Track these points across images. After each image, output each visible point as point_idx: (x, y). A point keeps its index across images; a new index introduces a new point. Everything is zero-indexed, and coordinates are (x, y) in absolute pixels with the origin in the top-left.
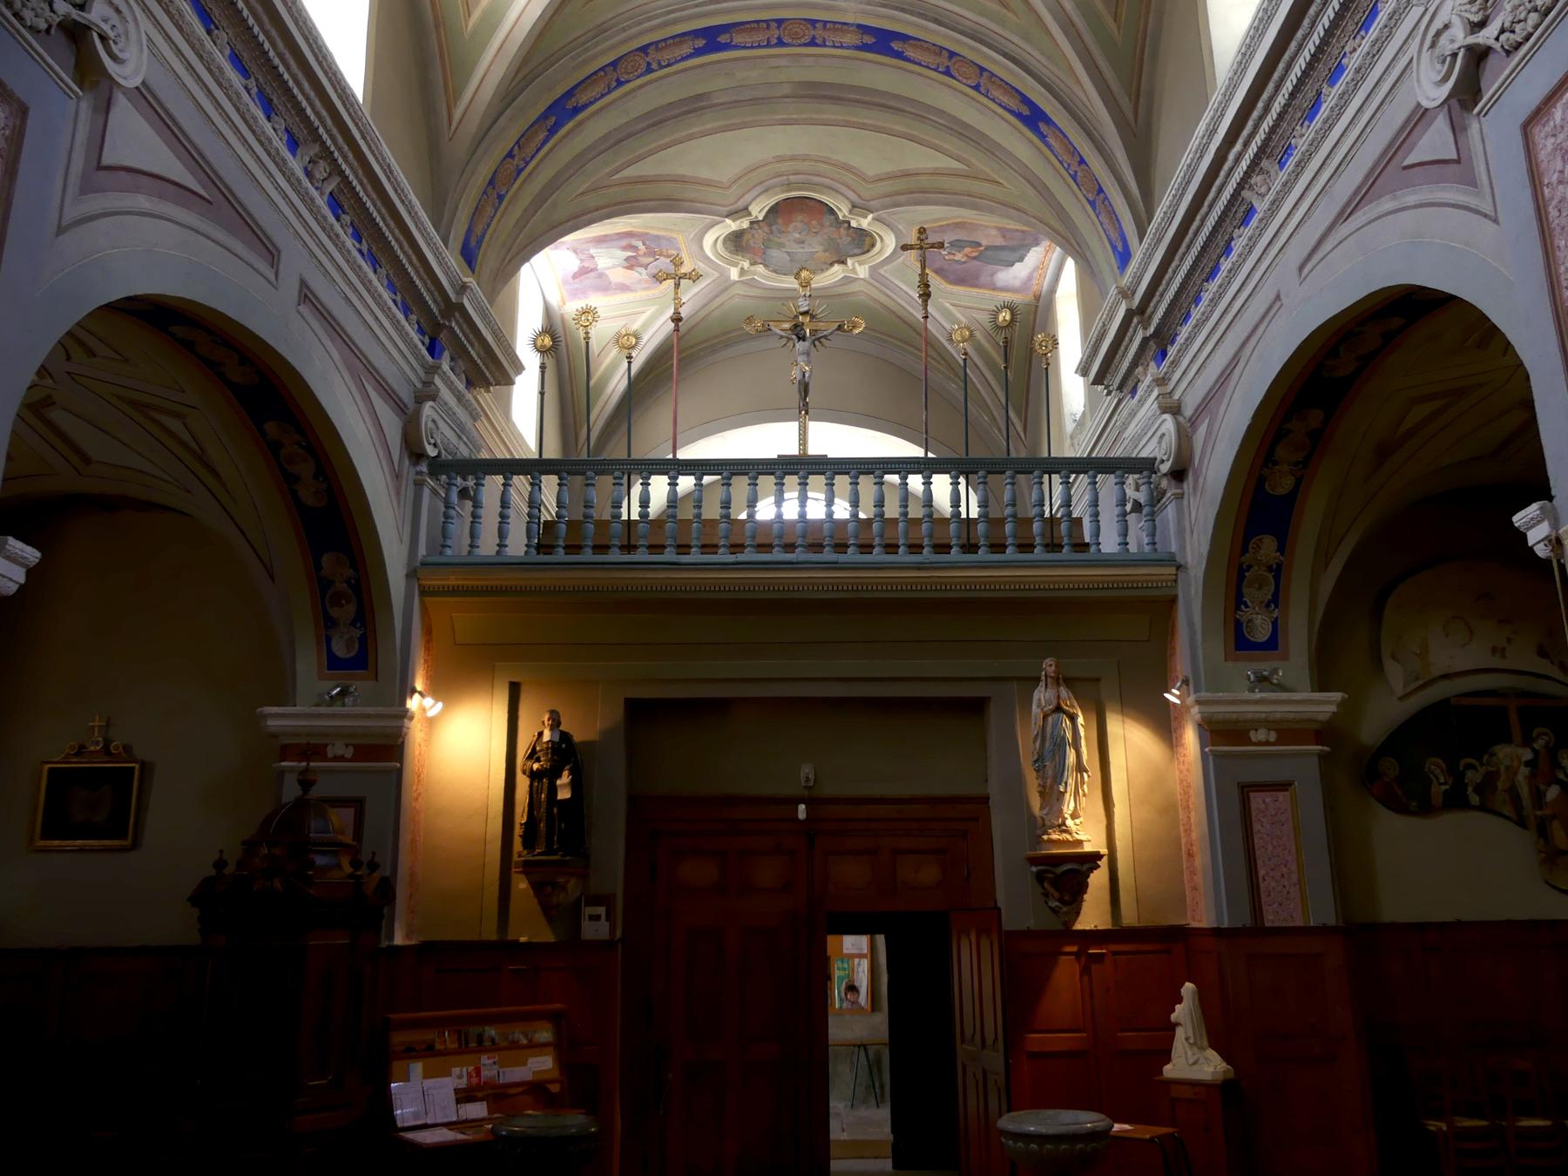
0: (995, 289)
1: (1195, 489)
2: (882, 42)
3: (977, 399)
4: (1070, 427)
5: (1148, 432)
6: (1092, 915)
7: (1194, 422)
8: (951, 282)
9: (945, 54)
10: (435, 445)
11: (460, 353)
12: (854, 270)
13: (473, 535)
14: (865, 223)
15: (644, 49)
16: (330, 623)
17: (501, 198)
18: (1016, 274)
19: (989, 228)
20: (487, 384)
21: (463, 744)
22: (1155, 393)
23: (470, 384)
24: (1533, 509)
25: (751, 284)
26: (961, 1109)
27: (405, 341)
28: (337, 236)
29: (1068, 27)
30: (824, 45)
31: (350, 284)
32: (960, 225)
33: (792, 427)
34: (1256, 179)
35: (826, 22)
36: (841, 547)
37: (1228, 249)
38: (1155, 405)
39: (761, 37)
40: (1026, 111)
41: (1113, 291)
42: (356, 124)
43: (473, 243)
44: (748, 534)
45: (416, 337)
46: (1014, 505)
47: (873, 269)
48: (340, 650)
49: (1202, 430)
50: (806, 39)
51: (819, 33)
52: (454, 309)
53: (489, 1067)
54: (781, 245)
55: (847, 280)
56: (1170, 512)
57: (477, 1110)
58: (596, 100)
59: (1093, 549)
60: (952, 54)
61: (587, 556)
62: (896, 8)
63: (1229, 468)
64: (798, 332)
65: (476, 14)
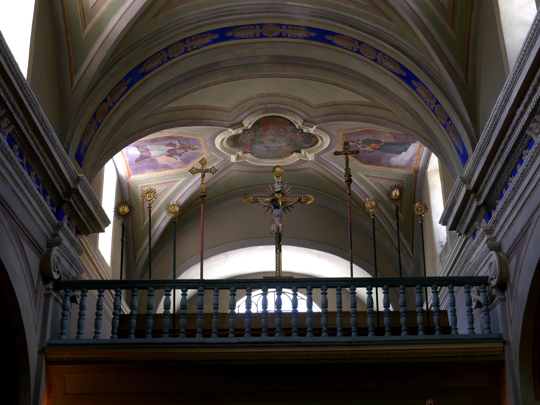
0: (391, 166)
1: (511, 295)
2: (320, 36)
3: (381, 232)
4: (439, 250)
5: (484, 262)
7: (509, 255)
8: (364, 163)
9: (357, 43)
10: (58, 272)
11: (74, 215)
12: (305, 156)
13: (79, 326)
14: (312, 130)
15: (184, 41)
17: (99, 124)
18: (404, 157)
19: (386, 135)
20: (87, 233)
22: (486, 238)
23: (78, 233)
25: (244, 164)
27: (43, 212)
28: (12, 158)
30: (287, 37)
31: (16, 183)
32: (368, 132)
33: (271, 250)
34: (533, 125)
35: (287, 26)
36: (302, 332)
37: (521, 161)
38: (486, 246)
39: (251, 33)
40: (404, 74)
41: (458, 179)
42: (26, 98)
43: (82, 151)
44: (246, 325)
45: (49, 208)
46: (405, 306)
47: (317, 156)
49: (514, 261)
50: (277, 34)
51: (284, 31)
54: (261, 143)
55: (301, 162)
56: (498, 308)
58: (155, 68)
59: (453, 332)
60: (361, 43)
61: (149, 339)
62: (328, 19)
63: (530, 285)
64: (274, 203)
65: (89, 27)
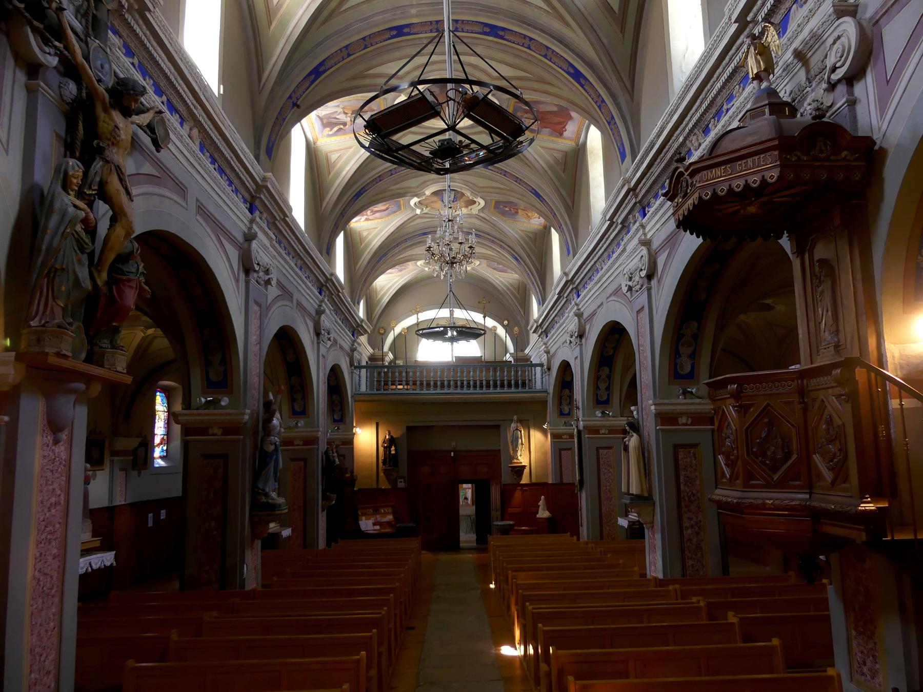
6: (525, 480)
21: (366, 439)
29: (523, 248)
33: (448, 310)
48: (336, 417)
52: (261, 187)
53: (379, 518)
57: (377, 527)
65: (274, 25)
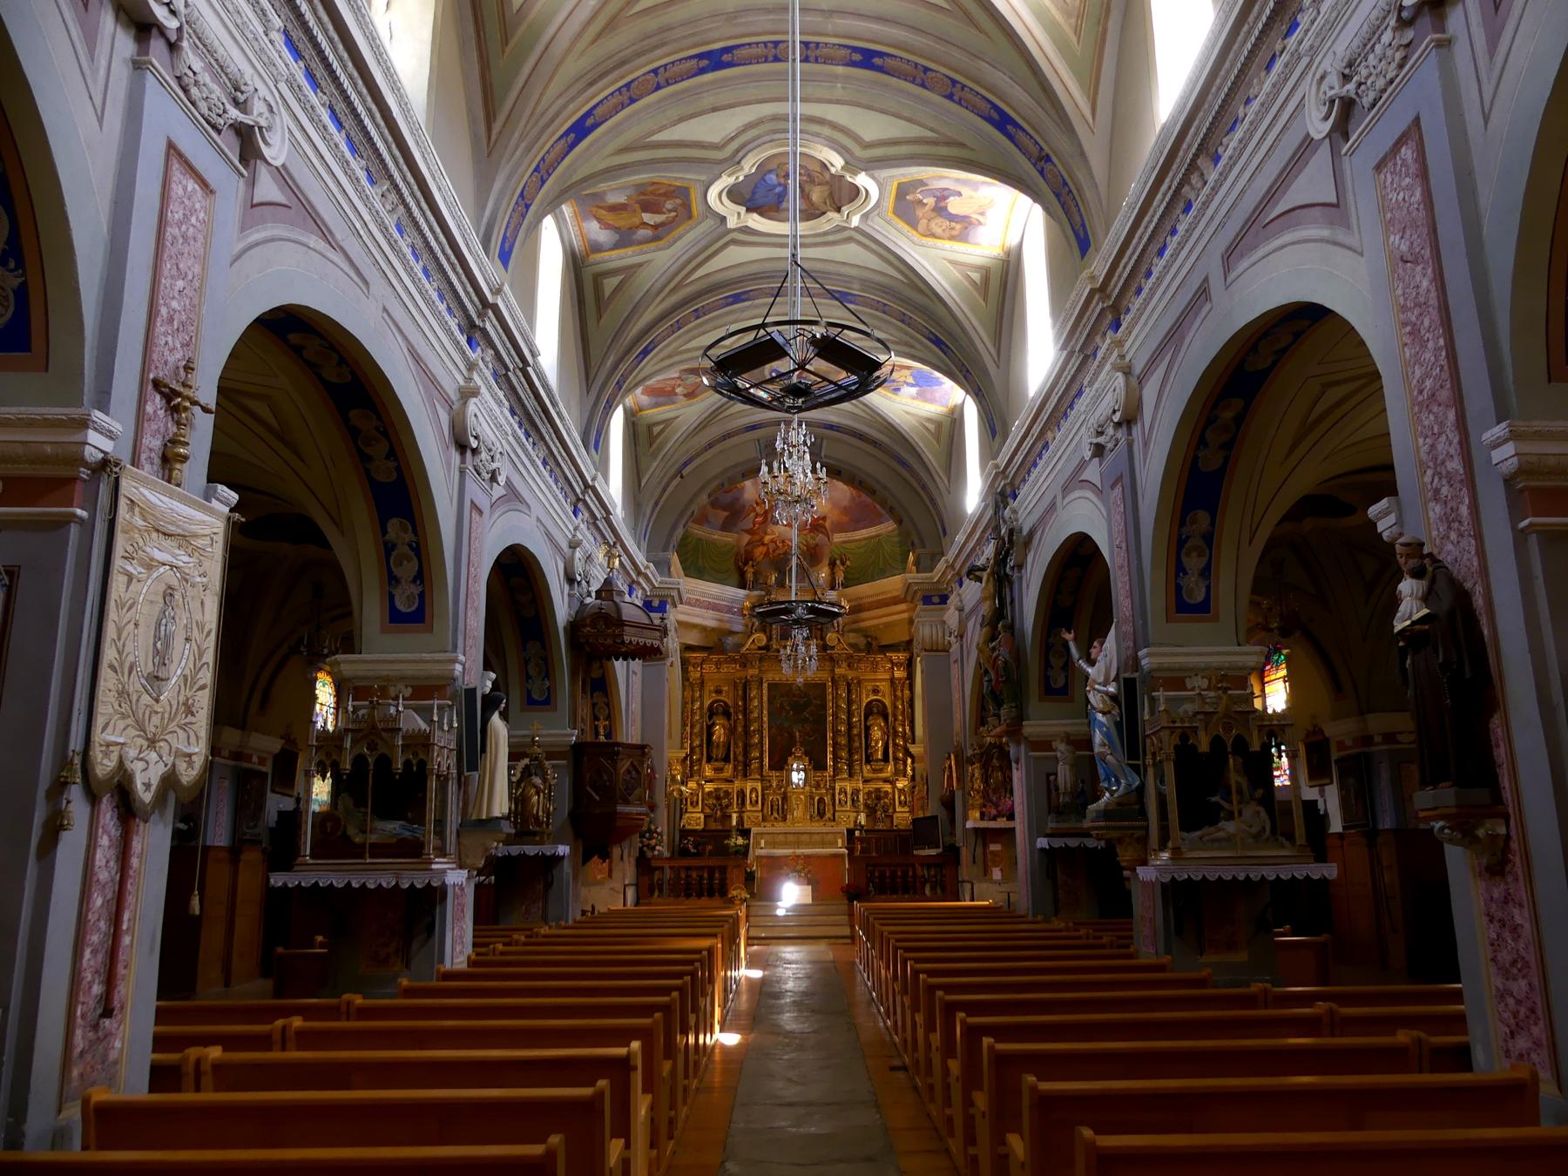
7: (1141, 382)
16: (393, 579)
24: (1384, 503)
26: (526, 70)
48: (402, 606)
